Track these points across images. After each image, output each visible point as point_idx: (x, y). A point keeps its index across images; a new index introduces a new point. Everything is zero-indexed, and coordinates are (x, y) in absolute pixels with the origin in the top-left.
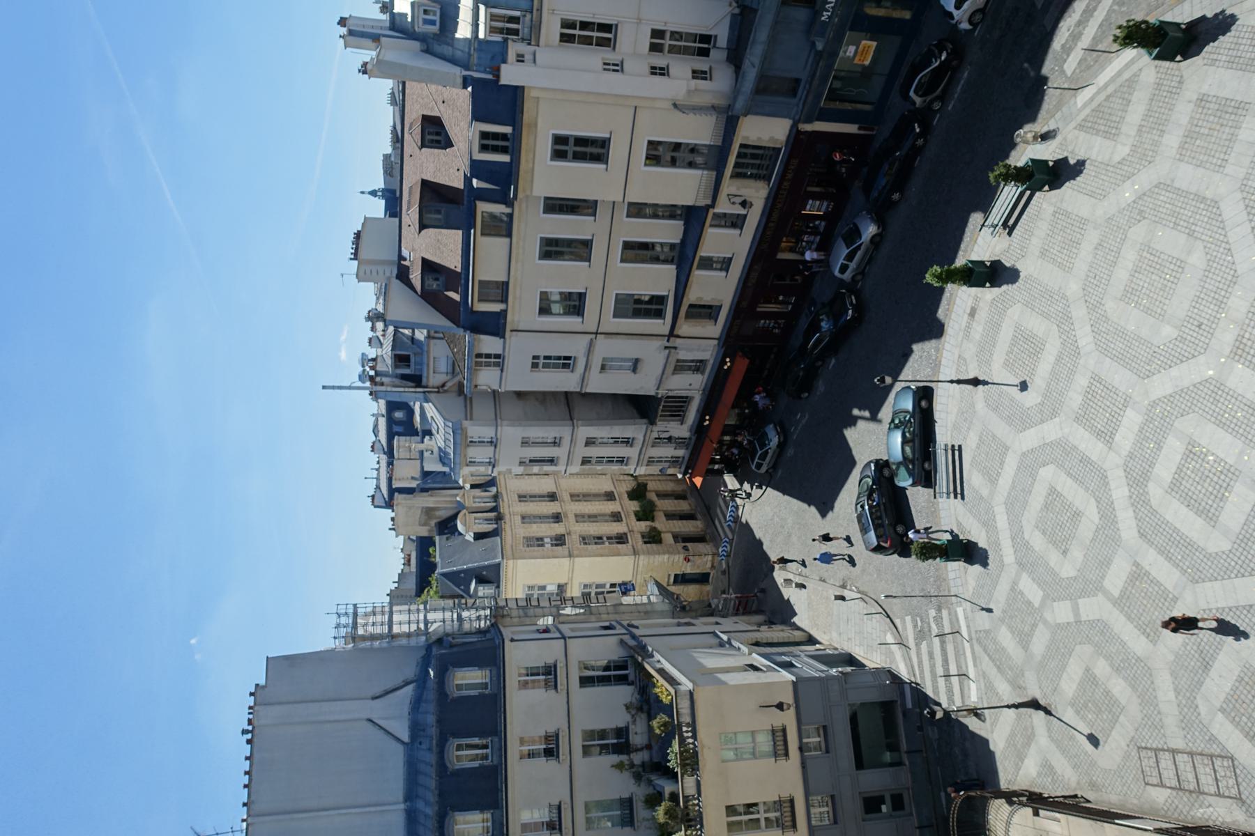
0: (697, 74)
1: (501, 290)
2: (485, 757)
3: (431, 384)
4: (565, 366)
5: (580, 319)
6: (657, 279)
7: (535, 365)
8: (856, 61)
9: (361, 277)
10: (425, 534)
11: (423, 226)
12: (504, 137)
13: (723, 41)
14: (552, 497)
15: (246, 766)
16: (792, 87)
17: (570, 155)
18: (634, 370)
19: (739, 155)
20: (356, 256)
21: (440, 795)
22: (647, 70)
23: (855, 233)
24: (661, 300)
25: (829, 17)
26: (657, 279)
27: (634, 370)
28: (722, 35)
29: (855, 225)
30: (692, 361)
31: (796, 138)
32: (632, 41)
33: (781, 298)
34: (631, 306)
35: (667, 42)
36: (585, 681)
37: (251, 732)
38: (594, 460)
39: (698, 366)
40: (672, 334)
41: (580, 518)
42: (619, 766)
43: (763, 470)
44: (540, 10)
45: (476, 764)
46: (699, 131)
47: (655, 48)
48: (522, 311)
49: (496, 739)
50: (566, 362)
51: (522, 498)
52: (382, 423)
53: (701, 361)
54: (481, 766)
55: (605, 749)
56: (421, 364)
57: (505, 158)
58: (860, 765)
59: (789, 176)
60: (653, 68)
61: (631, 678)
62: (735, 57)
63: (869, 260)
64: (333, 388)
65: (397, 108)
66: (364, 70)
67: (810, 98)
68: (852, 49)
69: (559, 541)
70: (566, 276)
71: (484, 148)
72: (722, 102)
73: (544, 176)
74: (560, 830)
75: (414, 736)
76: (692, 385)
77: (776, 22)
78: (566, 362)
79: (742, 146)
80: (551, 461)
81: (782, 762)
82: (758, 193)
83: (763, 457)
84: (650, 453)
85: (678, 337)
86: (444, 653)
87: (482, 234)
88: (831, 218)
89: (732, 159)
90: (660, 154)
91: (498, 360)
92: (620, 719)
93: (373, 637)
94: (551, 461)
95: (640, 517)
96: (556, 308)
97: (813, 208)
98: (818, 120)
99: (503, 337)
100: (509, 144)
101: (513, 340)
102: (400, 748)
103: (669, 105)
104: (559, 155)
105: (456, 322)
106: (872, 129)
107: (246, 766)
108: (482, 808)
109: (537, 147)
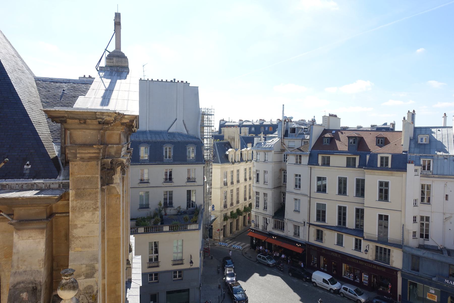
0: (414, 233)
1: (326, 163)
2: (166, 157)
3: (285, 140)
4: (296, 186)
5: (316, 191)
6: (332, 218)
7: (296, 175)
8: (428, 294)
9: (324, 117)
10: (225, 138)
11: (349, 138)
12: (387, 165)
13: (427, 243)
14: (238, 181)
15: (164, 80)
16: (415, 269)
17: (381, 188)
18: (295, 211)
19: (385, 249)
20: (331, 115)
21: (155, 142)
22: (415, 215)
23: (360, 294)
24: (324, 220)
25: (446, 283)
26: (332, 218)
27: (295, 211)
28: (429, 243)
29: (362, 294)
30: (299, 232)
31: (394, 271)
32: (424, 210)
33: (326, 265)
34: (321, 209)
35: (425, 222)
36: (189, 192)
37: (174, 82)
38: (258, 196)
39: (297, 234)
40: (310, 224)
41: (232, 191)
42: (160, 204)
43: (258, 258)
44: (434, 177)
45: (164, 154)
46: (393, 234)
47: (422, 218)
48: (319, 171)
49: (172, 161)
50: (298, 186)
51: (238, 171)
52: (250, 123)
53: (299, 235)
54: (163, 156)
55: (166, 199)
56: (292, 137)
57: (379, 165)
58: (168, 293)
59: (378, 268)
60: (415, 217)
61: (189, 209)
62: (421, 247)
63: (349, 299)
64: (283, 108)
65: (356, 129)
66: (404, 118)
67: (412, 276)
68: (433, 292)
69: (225, 184)
70: (332, 186)
71: (382, 158)
72: (405, 244)
73: (372, 180)
74: (141, 183)
75: (170, 134)
76: (289, 232)
77: (442, 262)
78: (298, 186)
79: (389, 250)
80: (258, 181)
81: (171, 263)
82: (370, 256)
83: (263, 258)
84: (261, 217)
85: (309, 227)
86: (198, 144)
87: (347, 158)
88: (361, 285)
89: (384, 246)
90: (383, 219)
91: (298, 162)
92: (176, 204)
93: (203, 120)
94: (258, 181)
95: (232, 213)
96: (320, 183)
97: (365, 277)
98: (402, 279)
99: (308, 164)
100: (384, 167)
101: (307, 168)
102: (166, 129)
103: (403, 223)
104: (381, 184)
105: (313, 148)
106: (400, 300)
107: (164, 80)
108: (150, 156)
109: (384, 177)
